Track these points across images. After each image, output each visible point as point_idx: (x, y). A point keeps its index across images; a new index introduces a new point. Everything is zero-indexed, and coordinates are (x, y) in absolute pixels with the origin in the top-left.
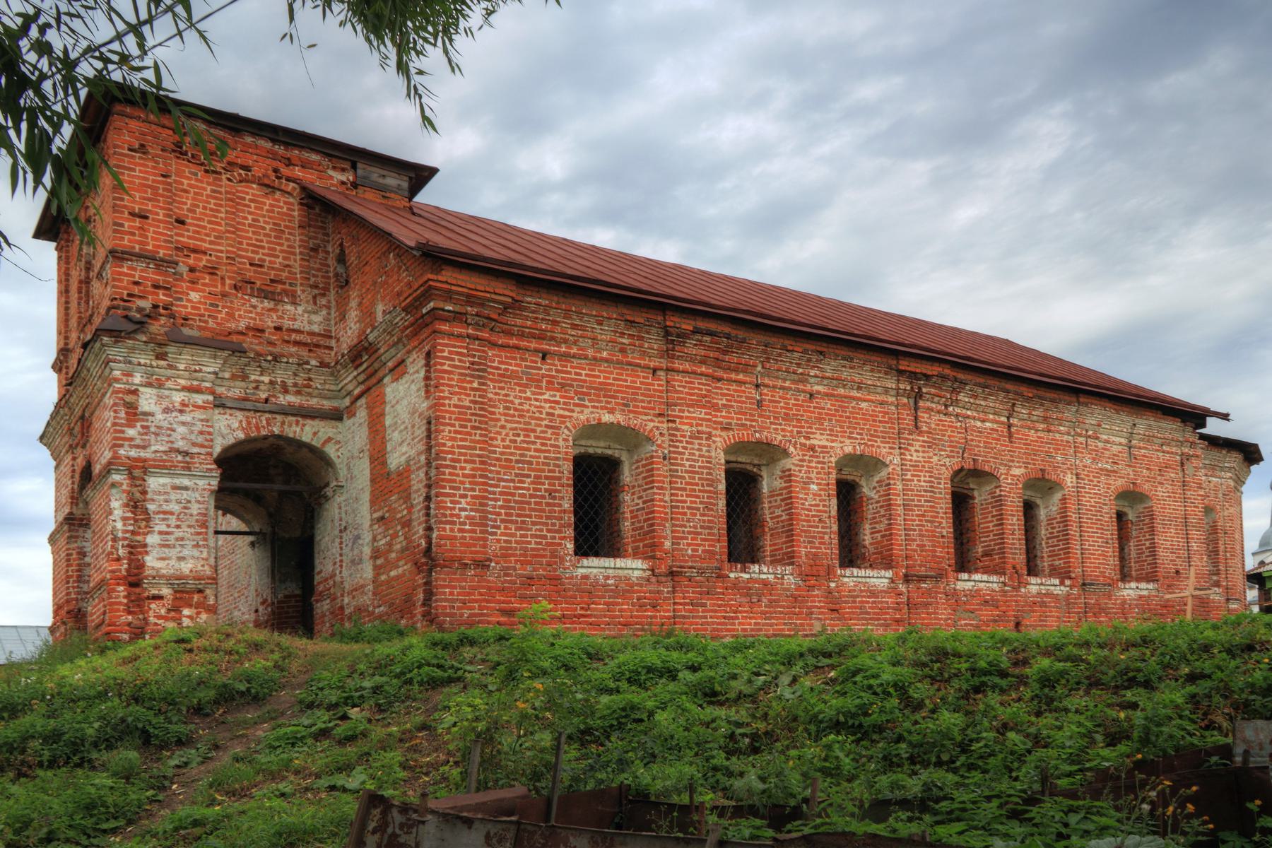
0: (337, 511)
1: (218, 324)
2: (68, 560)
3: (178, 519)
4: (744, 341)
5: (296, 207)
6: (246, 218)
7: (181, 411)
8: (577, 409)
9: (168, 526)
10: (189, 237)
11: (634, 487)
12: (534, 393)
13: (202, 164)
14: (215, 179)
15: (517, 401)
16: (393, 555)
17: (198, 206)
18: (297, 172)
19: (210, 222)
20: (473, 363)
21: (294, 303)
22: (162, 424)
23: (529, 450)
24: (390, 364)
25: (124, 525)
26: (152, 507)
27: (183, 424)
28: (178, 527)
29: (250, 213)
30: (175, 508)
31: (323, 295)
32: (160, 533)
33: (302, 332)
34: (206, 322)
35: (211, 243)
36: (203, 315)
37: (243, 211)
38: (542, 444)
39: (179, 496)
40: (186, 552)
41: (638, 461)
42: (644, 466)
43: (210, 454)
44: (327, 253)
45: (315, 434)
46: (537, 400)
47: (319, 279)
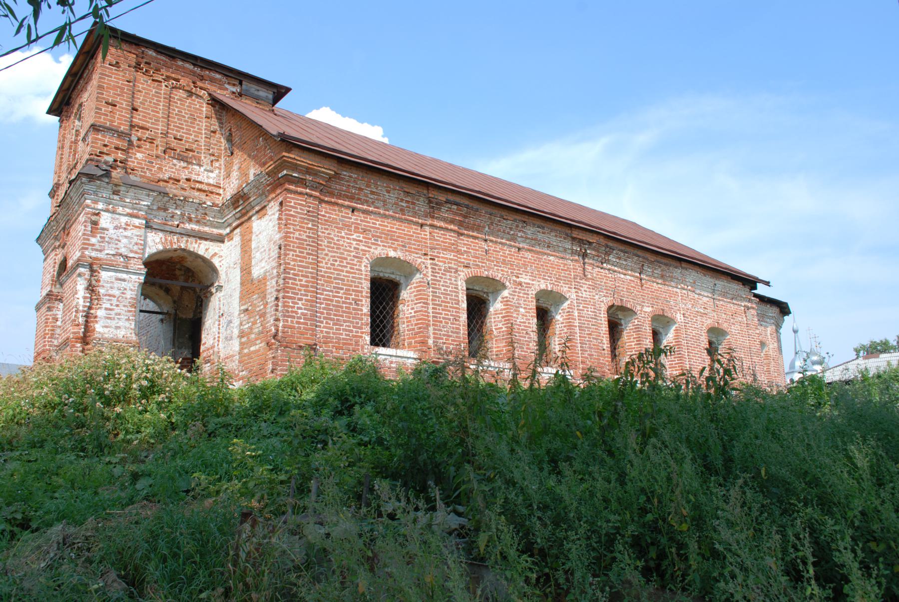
0: (218, 303)
3: (118, 300)
7: (125, 229)
8: (373, 247)
9: (111, 305)
12: (346, 234)
15: (336, 238)
16: (253, 336)
22: (112, 236)
23: (342, 271)
26: (102, 291)
27: (126, 237)
28: (117, 306)
30: (116, 292)
34: (145, 173)
35: (152, 123)
38: (351, 268)
40: (121, 324)
46: (348, 238)
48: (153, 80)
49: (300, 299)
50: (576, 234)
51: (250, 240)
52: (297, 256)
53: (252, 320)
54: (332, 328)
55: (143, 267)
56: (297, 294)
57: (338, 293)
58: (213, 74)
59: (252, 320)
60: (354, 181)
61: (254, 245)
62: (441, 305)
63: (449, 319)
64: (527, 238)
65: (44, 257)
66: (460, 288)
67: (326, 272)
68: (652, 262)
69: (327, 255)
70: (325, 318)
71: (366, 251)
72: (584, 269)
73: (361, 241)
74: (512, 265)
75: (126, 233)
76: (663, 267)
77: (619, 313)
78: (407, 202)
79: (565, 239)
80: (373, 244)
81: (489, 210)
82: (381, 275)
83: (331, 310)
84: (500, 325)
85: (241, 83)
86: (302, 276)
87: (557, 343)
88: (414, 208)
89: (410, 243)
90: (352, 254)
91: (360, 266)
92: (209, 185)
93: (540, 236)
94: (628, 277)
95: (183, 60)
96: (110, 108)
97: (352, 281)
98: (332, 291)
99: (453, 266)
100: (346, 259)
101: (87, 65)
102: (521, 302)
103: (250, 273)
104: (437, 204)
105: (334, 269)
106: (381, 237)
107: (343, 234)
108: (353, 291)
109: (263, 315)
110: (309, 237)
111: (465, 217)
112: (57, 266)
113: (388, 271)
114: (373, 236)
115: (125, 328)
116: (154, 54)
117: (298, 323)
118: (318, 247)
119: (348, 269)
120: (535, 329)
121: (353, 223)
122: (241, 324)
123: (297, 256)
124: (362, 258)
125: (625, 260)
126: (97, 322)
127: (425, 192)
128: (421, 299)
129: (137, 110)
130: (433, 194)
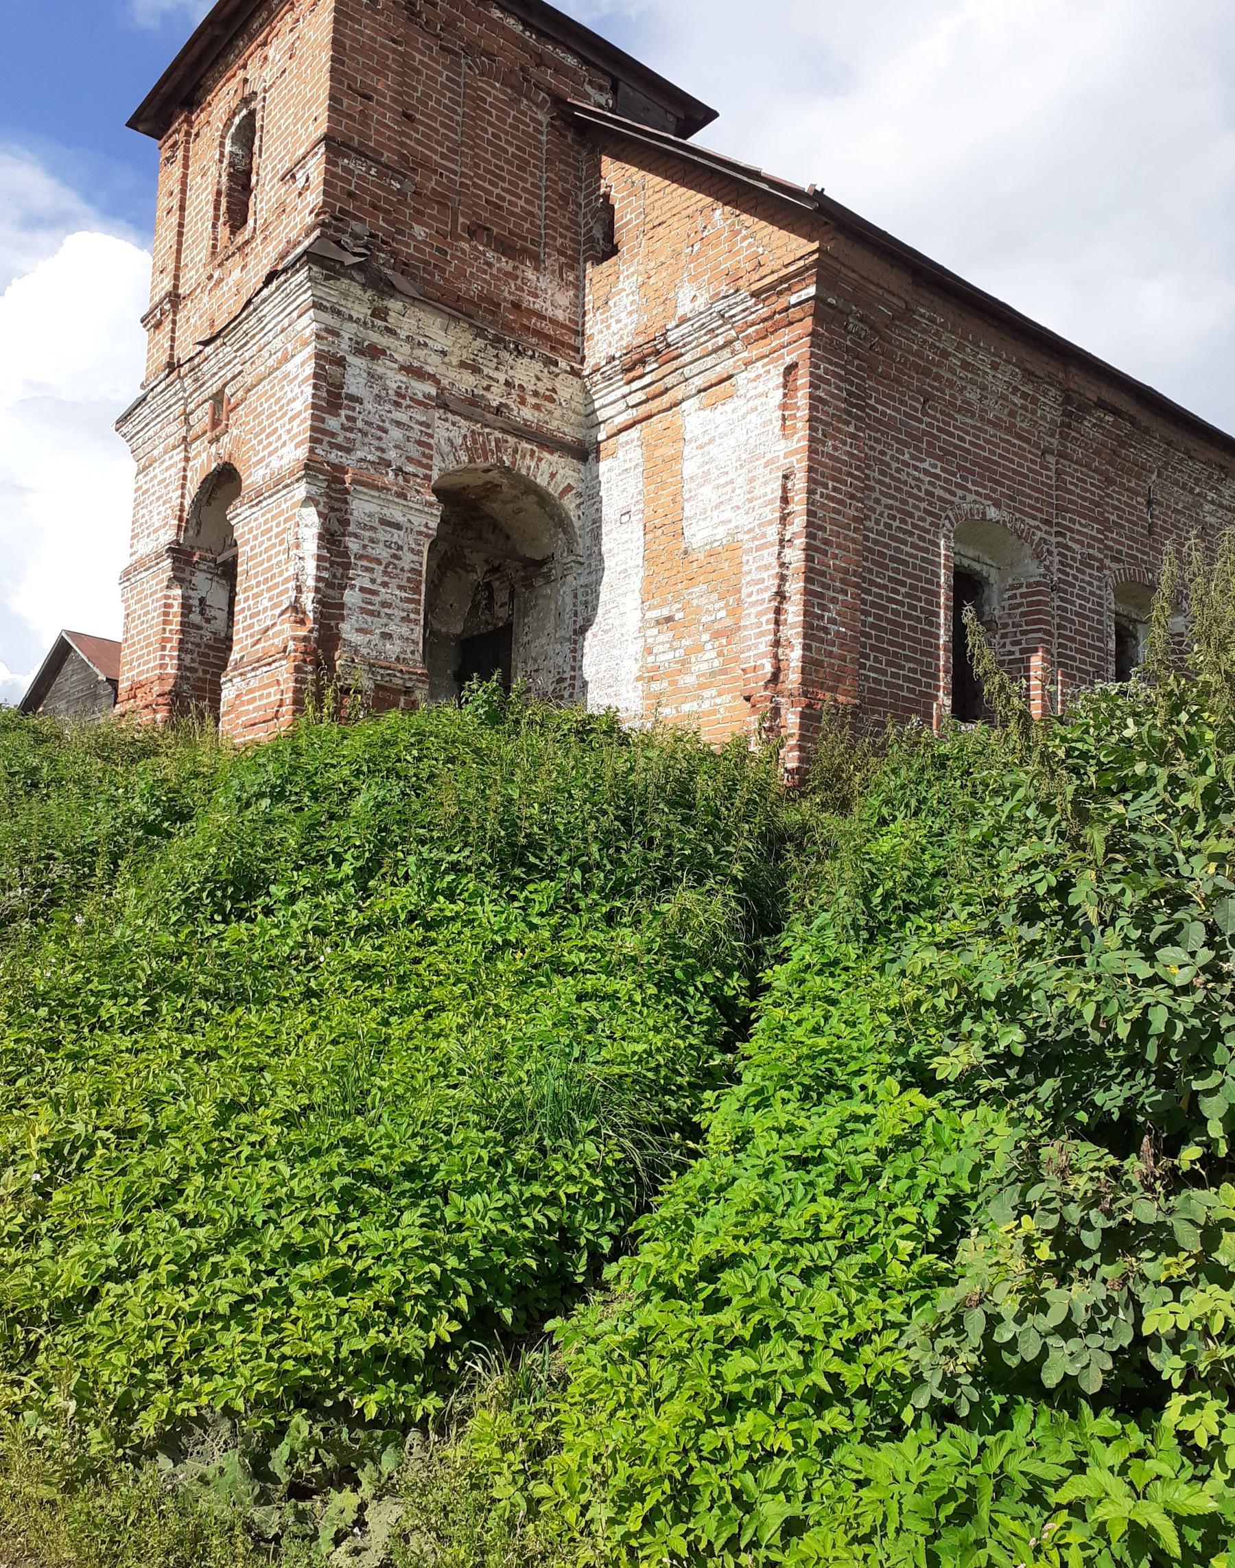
0: (569, 600)
1: (445, 279)
2: (166, 614)
3: (385, 573)
4: (1146, 431)
5: (544, 130)
6: (486, 131)
7: (397, 404)
8: (960, 492)
9: (373, 581)
10: (417, 141)
11: (1005, 626)
12: (913, 457)
13: (438, 36)
14: (452, 61)
15: (894, 465)
16: (690, 680)
17: (430, 98)
18: (549, 76)
19: (443, 125)
20: (850, 393)
21: (537, 269)
22: (371, 418)
23: (905, 543)
24: (699, 382)
25: (318, 568)
26: (353, 545)
27: (398, 424)
28: (385, 585)
29: (490, 124)
30: (384, 554)
31: (572, 268)
32: (362, 589)
33: (544, 318)
34: (432, 275)
35: (443, 156)
36: (427, 263)
37: (483, 120)
38: (921, 538)
39: (388, 537)
40: (392, 628)
41: (1012, 587)
42: (1023, 595)
43: (427, 478)
44: (579, 206)
45: (553, 476)
46: (916, 468)
47: (567, 242)
48: (442, 47)
49: (834, 600)
54: (884, 673)
58: (561, 54)
59: (686, 642)
60: (937, 334)
61: (689, 468)
70: (873, 648)
78: (1024, 396)
80: (958, 485)
86: (839, 546)
88: (1034, 412)
90: (923, 505)
91: (936, 534)
92: (553, 321)
95: (503, 9)
100: (911, 515)
105: (891, 537)
106: (973, 473)
112: (193, 488)
113: (971, 553)
114: (960, 467)
115: (401, 637)
119: (915, 540)
123: (829, 497)
126: (342, 618)
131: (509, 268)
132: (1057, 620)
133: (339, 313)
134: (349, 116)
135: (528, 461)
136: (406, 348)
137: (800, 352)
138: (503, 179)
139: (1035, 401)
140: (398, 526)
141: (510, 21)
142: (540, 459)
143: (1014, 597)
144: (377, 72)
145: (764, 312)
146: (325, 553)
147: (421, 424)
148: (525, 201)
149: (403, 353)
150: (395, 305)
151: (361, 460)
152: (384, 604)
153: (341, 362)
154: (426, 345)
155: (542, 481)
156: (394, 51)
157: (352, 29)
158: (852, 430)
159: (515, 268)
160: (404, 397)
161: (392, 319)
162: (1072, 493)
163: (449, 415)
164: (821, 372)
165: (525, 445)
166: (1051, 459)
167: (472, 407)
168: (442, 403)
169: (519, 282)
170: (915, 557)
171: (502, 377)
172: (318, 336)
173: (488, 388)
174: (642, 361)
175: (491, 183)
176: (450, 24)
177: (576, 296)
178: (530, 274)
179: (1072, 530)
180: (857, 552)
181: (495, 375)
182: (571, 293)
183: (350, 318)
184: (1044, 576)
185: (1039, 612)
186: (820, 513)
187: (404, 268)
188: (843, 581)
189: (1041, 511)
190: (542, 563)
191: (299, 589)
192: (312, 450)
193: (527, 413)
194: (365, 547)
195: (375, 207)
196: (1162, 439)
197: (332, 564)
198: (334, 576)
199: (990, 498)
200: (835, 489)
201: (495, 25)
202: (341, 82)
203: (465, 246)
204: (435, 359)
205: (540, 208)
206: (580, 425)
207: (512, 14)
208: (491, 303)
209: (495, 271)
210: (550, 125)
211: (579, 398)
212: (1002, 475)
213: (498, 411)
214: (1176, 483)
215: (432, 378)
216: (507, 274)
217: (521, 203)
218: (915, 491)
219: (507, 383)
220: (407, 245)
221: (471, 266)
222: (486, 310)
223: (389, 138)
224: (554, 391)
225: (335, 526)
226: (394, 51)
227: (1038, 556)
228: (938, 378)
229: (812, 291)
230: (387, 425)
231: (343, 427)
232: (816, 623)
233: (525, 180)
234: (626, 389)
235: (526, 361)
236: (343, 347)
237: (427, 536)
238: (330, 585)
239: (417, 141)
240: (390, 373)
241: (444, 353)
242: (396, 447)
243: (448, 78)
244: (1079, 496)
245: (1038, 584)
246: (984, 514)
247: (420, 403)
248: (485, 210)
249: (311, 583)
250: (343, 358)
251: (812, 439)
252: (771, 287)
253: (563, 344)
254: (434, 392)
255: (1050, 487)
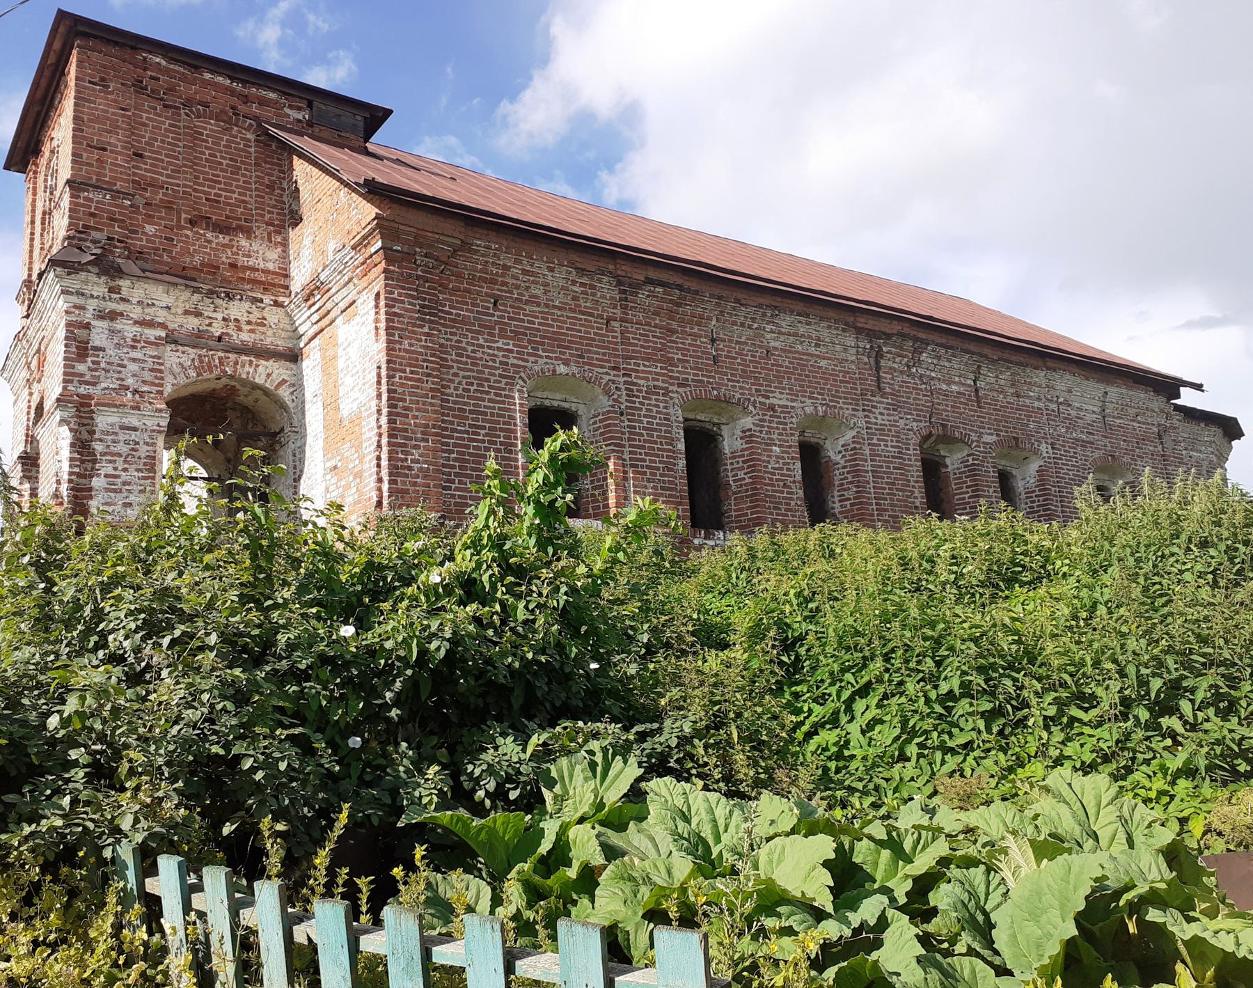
3: (125, 462)
7: (133, 347)
8: (532, 359)
10: (146, 170)
13: (162, 99)
15: (470, 348)
19: (166, 156)
20: (422, 306)
21: (249, 238)
25: (71, 466)
26: (98, 447)
27: (134, 360)
28: (125, 470)
30: (124, 449)
32: (106, 476)
33: (257, 270)
34: (161, 256)
35: (168, 176)
37: (201, 146)
38: (496, 394)
39: (127, 437)
40: (132, 498)
41: (595, 416)
42: (601, 421)
44: (283, 190)
45: (269, 375)
46: (489, 348)
49: (416, 447)
50: (861, 321)
51: (335, 357)
52: (406, 378)
53: (343, 483)
55: (164, 406)
56: (411, 439)
57: (478, 434)
59: (343, 483)
61: (341, 364)
62: (643, 447)
63: (658, 469)
64: (780, 333)
65: (14, 398)
66: (673, 418)
67: (455, 402)
68: (993, 361)
69: (456, 375)
70: (456, 475)
71: (520, 366)
72: (879, 378)
73: (511, 351)
74: (757, 378)
75: (133, 354)
76: (1015, 368)
77: (940, 447)
78: (582, 285)
79: (844, 330)
81: (717, 292)
82: (547, 403)
83: (468, 461)
84: (741, 474)
85: (310, 105)
86: (418, 410)
87: (836, 499)
88: (594, 295)
89: (589, 352)
91: (511, 390)
93: (802, 329)
94: (954, 387)
95: (211, 72)
96: (96, 154)
97: (498, 415)
98: (467, 432)
99: (660, 384)
101: (58, 86)
102: (775, 437)
103: (337, 409)
104: (630, 286)
107: (481, 341)
108: (501, 430)
109: (359, 475)
110: (427, 348)
111: (679, 305)
113: (558, 396)
114: (530, 342)
116: (164, 63)
117: (415, 484)
118: (443, 365)
120: (799, 478)
121: (496, 323)
122: (327, 490)
123: (406, 378)
124: (513, 378)
125: (949, 360)
126: (91, 497)
127: (611, 267)
128: (611, 438)
129: (141, 156)
130: (624, 269)
131: (226, 241)
132: (627, 435)
133: (83, 294)
134: (88, 164)
135: (247, 368)
136: (139, 309)
137: (379, 285)
138: (220, 182)
139: (593, 287)
140: (135, 429)
141: (220, 79)
142: (257, 366)
143: (595, 423)
144: (110, 132)
145: (361, 259)
146: (76, 455)
147: (153, 357)
148: (237, 193)
149: (137, 313)
150: (124, 283)
151: (107, 388)
152: (124, 483)
153: (87, 326)
154: (153, 304)
155: (259, 380)
156: (123, 116)
157: (89, 108)
158: (426, 330)
159: (231, 240)
160: (139, 342)
161: (125, 292)
162: (636, 345)
163: (180, 348)
164: (395, 296)
165: (244, 358)
166: (616, 324)
167: (197, 339)
168: (171, 339)
169: (235, 249)
170: (494, 408)
171: (219, 316)
172: (67, 312)
173: (210, 325)
174: (311, 294)
175: (209, 187)
176: (171, 90)
177: (284, 251)
178: (244, 243)
179: (637, 371)
180: (435, 412)
181: (214, 315)
182: (279, 250)
183: (92, 296)
184: (613, 406)
185: (610, 432)
186: (400, 390)
187: (137, 255)
188: (423, 433)
189: (609, 361)
190: (276, 434)
191: (58, 482)
192: (65, 388)
193: (245, 336)
194: (108, 446)
195: (112, 219)
196: (712, 296)
197: (83, 462)
198: (86, 470)
199: (561, 359)
200: (412, 372)
201: (206, 84)
202: (81, 144)
203: (188, 232)
204: (163, 313)
205: (251, 196)
206: (290, 338)
207: (220, 74)
208: (212, 268)
209: (214, 245)
210: (256, 140)
211: (286, 320)
212: (569, 342)
213: (220, 339)
214: (734, 323)
215: (163, 326)
216: (224, 245)
217: (236, 195)
218: (490, 363)
219: (224, 319)
220: (141, 240)
221: (194, 245)
222: (209, 273)
223: (121, 173)
224: (264, 318)
225: (85, 436)
226: (123, 116)
227: (607, 393)
228: (504, 284)
229: (379, 244)
230: (125, 362)
231: (90, 369)
232: (400, 464)
233: (238, 180)
234: (308, 313)
235: (236, 303)
236: (88, 316)
237: (159, 432)
238: (79, 475)
239: (146, 170)
240: (126, 327)
241: (168, 308)
242: (134, 375)
243: (170, 125)
244: (642, 346)
245: (609, 412)
246: (554, 371)
247: (152, 343)
248: (205, 205)
249: (66, 477)
250: (89, 323)
251: (389, 342)
252: (359, 243)
253: (274, 285)
254: (163, 334)
255: (616, 343)
